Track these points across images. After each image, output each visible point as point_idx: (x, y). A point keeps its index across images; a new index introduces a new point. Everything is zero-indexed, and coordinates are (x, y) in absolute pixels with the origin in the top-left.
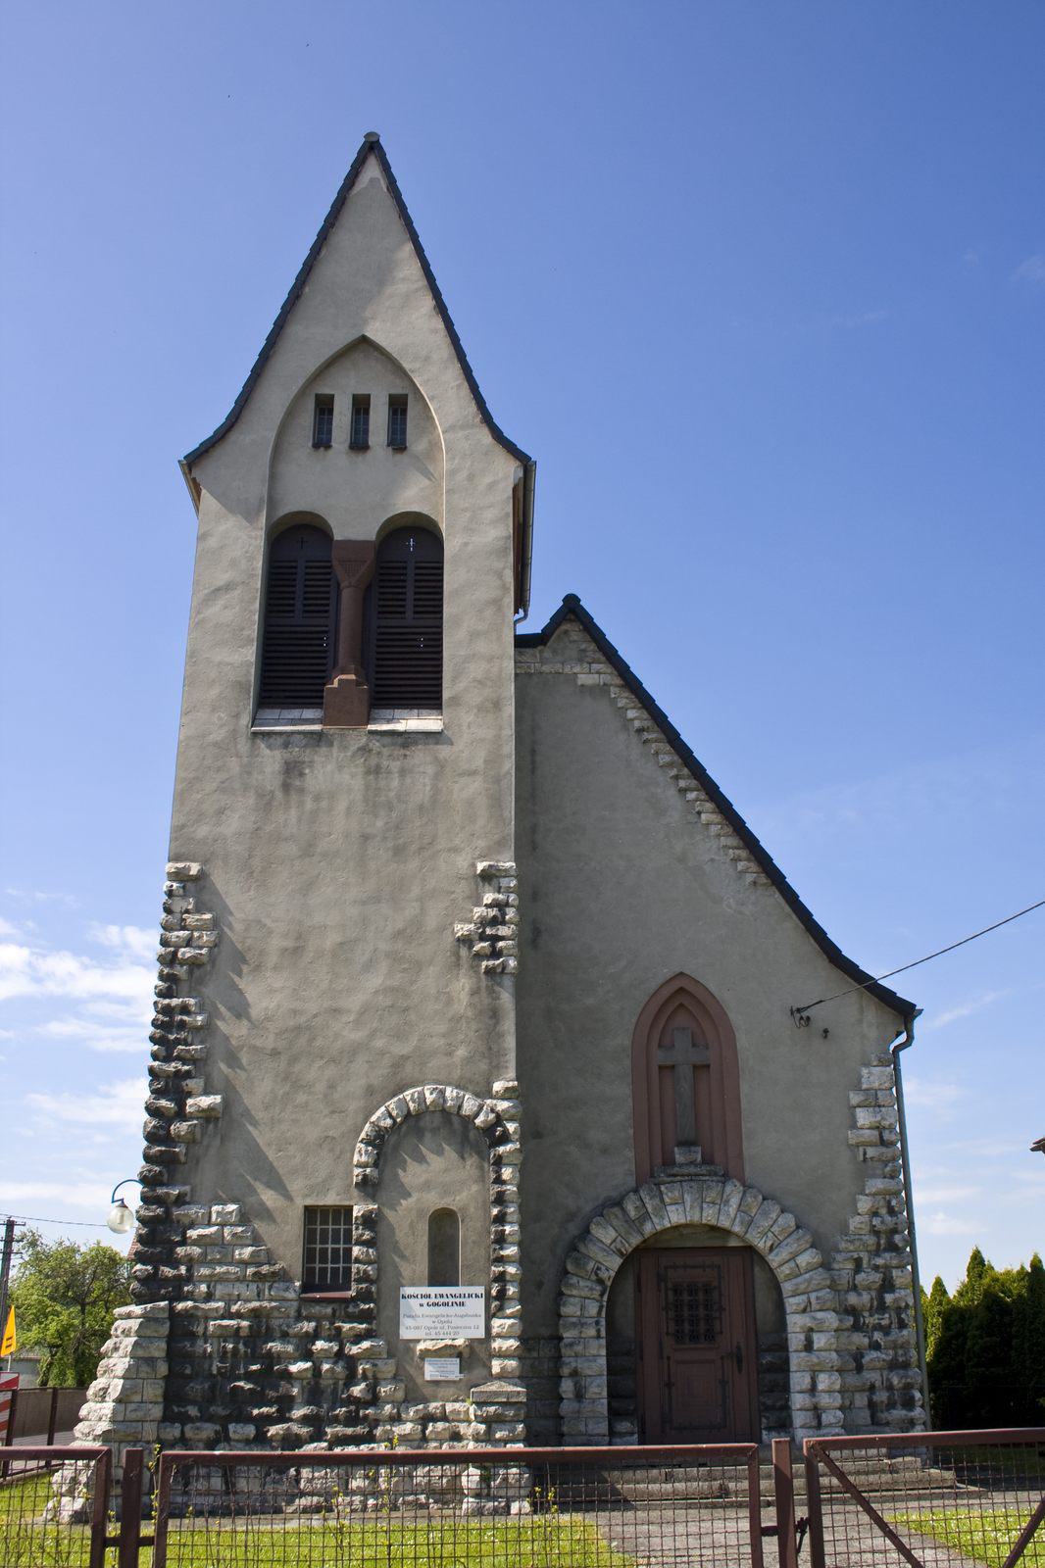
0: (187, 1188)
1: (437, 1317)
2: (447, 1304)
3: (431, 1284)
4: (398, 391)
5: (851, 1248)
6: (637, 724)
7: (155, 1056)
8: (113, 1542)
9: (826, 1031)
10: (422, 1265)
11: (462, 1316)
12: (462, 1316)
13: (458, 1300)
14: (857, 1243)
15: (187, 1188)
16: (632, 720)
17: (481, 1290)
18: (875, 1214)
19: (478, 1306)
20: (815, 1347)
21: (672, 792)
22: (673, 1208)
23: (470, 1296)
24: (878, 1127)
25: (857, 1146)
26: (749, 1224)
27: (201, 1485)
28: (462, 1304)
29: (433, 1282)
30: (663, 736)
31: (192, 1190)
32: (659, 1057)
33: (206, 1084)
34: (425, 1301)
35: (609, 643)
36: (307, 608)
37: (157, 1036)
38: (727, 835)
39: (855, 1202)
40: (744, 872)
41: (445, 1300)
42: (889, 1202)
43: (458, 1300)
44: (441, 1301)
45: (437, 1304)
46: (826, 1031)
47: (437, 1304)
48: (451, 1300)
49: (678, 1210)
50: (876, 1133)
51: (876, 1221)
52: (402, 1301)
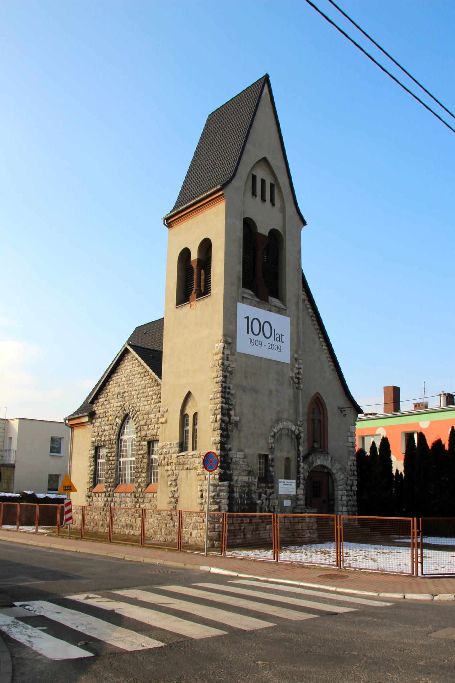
0: (231, 446)
2: (288, 485)
4: (272, 182)
6: (311, 314)
7: (222, 403)
10: (283, 474)
13: (291, 484)
15: (231, 446)
16: (310, 312)
17: (294, 481)
18: (351, 466)
19: (294, 485)
20: (343, 500)
21: (317, 337)
25: (349, 447)
26: (332, 466)
27: (239, 537)
28: (291, 485)
29: (285, 478)
31: (232, 446)
33: (235, 413)
34: (284, 483)
37: (223, 396)
38: (330, 358)
39: (347, 462)
40: (331, 365)
41: (288, 483)
42: (354, 463)
43: (291, 484)
46: (345, 415)
48: (289, 483)
49: (319, 461)
51: (352, 468)
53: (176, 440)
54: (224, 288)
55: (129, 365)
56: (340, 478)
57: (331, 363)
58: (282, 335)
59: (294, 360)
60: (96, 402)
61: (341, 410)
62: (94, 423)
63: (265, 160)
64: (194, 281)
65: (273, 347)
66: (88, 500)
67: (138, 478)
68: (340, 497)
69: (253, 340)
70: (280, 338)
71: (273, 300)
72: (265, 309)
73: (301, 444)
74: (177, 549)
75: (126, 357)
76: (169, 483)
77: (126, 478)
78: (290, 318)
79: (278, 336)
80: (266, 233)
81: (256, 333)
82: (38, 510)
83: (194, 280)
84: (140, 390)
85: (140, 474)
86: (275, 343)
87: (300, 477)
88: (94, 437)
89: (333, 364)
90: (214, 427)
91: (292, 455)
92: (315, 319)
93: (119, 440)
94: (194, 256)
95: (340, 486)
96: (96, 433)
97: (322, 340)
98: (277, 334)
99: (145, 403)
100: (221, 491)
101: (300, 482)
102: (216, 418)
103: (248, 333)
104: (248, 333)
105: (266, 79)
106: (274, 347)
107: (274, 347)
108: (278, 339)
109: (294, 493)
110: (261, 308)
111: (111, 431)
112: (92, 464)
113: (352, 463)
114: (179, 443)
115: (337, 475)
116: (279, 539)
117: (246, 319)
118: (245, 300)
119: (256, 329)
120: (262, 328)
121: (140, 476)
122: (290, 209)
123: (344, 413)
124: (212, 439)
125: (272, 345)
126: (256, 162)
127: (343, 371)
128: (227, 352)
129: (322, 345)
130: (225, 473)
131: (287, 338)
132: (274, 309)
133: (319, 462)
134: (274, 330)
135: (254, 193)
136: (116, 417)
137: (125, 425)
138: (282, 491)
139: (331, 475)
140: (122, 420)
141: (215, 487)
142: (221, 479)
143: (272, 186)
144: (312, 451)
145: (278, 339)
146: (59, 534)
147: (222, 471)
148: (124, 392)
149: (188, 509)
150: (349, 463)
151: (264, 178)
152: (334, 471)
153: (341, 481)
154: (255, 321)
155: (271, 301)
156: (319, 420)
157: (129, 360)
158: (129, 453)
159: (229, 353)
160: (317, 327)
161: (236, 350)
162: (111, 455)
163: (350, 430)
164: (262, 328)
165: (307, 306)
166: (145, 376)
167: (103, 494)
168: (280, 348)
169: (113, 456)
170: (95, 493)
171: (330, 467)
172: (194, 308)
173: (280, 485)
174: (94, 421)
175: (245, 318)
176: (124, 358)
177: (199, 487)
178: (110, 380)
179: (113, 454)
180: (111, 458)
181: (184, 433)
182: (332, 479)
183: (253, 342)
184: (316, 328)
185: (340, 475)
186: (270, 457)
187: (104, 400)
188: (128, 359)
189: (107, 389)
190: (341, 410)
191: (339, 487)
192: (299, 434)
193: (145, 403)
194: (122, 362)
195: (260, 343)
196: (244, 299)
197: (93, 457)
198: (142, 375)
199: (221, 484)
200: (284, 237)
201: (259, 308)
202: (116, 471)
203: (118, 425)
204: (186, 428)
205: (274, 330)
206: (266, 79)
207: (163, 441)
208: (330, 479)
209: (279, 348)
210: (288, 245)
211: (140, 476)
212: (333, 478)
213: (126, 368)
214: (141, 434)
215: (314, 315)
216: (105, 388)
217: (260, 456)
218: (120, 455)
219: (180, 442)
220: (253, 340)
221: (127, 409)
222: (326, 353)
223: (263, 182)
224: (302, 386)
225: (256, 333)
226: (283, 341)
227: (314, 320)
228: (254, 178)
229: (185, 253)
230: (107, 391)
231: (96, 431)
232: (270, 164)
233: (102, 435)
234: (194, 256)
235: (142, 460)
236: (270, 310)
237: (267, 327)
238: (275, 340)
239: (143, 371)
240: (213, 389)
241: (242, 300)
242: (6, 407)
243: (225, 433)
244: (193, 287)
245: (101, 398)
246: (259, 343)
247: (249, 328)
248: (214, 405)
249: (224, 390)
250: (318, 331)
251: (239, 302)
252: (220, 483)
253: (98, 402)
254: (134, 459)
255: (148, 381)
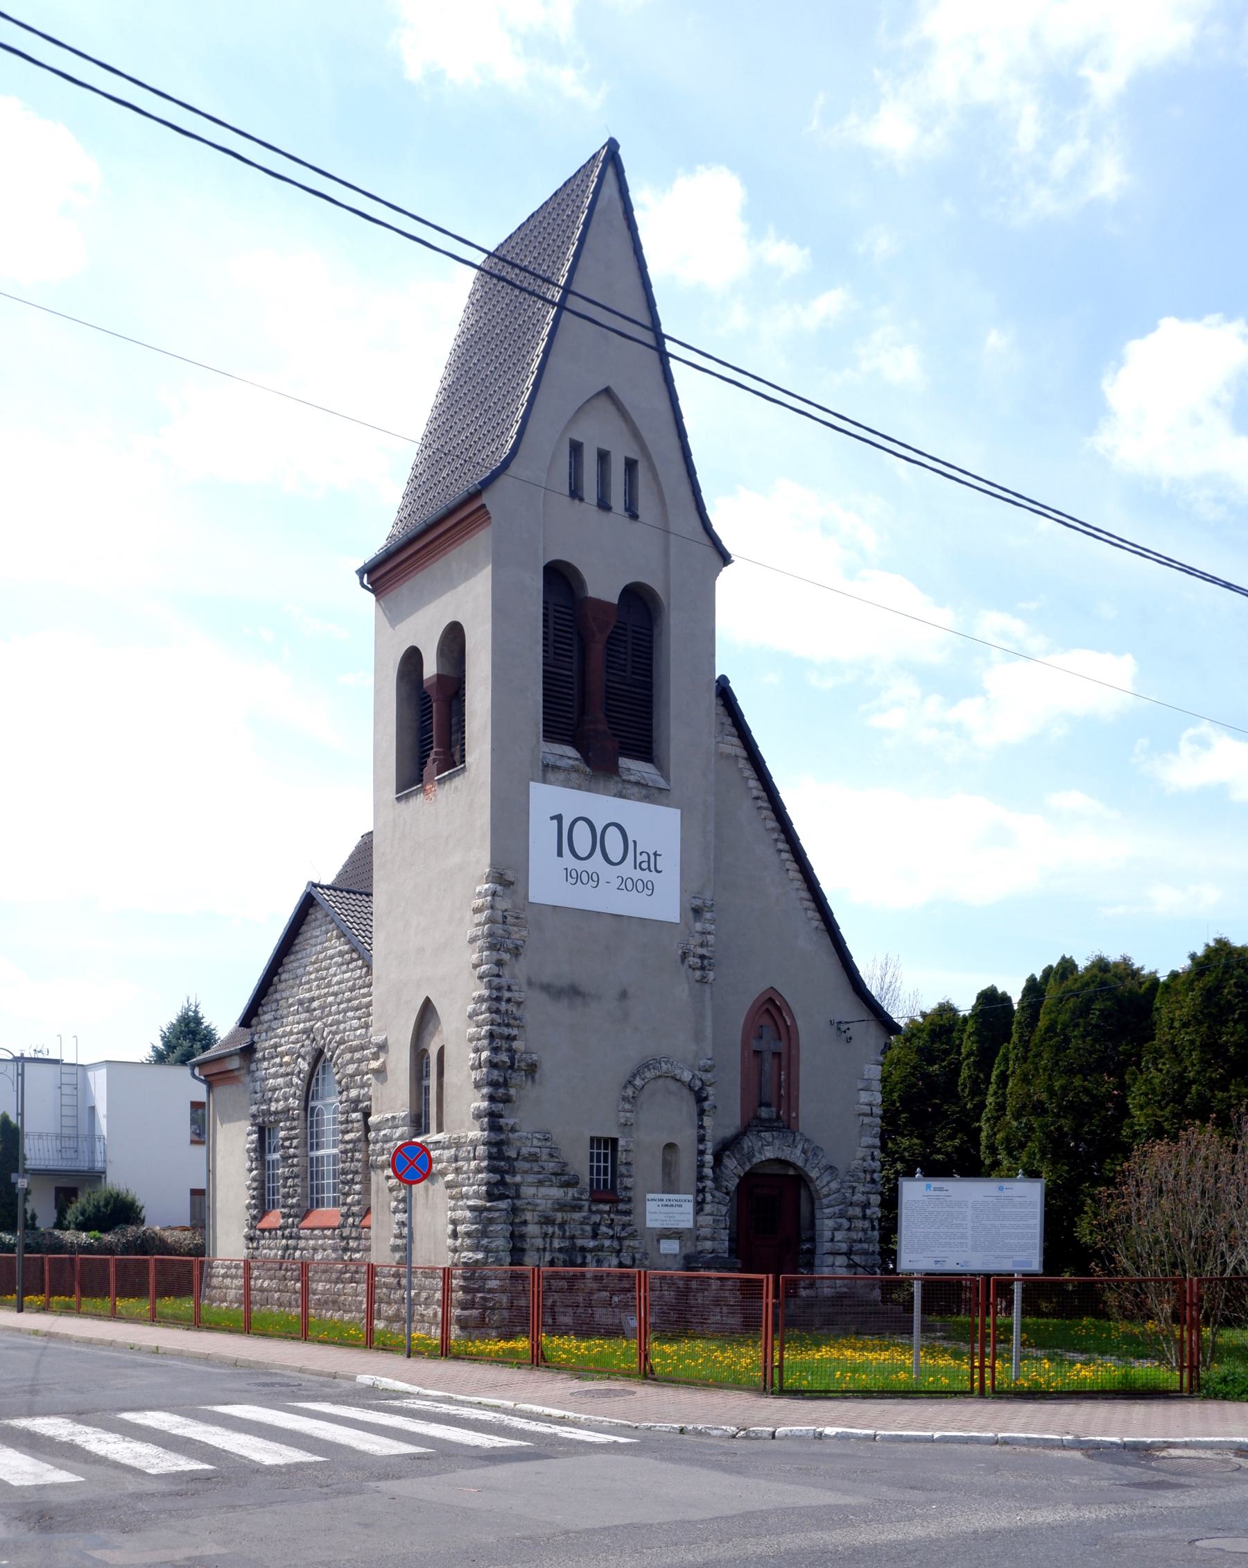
1: (667, 1213)
2: (672, 1206)
3: (663, 1192)
4: (632, 456)
5: (852, 1180)
6: (755, 793)
8: (777, 1366)
9: (851, 1038)
11: (681, 1213)
12: (681, 1213)
13: (679, 1203)
14: (856, 1177)
15: (517, 1120)
16: (751, 788)
17: (690, 1197)
19: (689, 1207)
20: (836, 1240)
22: (769, 1148)
23: (685, 1201)
24: (870, 1105)
28: (681, 1206)
30: (770, 806)
32: (755, 1045)
34: (660, 1203)
35: (492, 698)
36: (636, 653)
37: (494, 1007)
41: (671, 1203)
42: (873, 1153)
43: (679, 1203)
44: (669, 1203)
45: (667, 1205)
46: (851, 1038)
47: (667, 1205)
48: (674, 1203)
50: (869, 1108)
52: (647, 1202)
53: (404, 1109)
54: (493, 750)
55: (318, 933)
56: (830, 1190)
57: (811, 914)
58: (655, 854)
59: (691, 915)
60: (254, 1021)
61: (840, 1028)
62: (254, 1071)
63: (607, 392)
64: (434, 733)
65: (630, 886)
66: (250, 1246)
67: (347, 1194)
68: (828, 1234)
69: (573, 872)
70: (651, 862)
71: (633, 767)
72: (606, 792)
73: (706, 1113)
74: (300, 1336)
75: (311, 914)
76: (394, 1204)
77: (325, 1195)
78: (679, 811)
79: (645, 857)
80: (613, 597)
81: (583, 854)
82: (112, 1269)
83: (432, 731)
84: (344, 994)
85: (350, 1187)
86: (638, 874)
87: (704, 1187)
88: (256, 1104)
89: (817, 915)
90: (475, 1079)
91: (685, 1138)
92: (766, 805)
93: (307, 1108)
94: (430, 668)
95: (828, 1207)
96: (258, 1095)
97: (785, 856)
98: (641, 854)
99: (355, 1023)
100: (491, 1221)
101: (704, 1201)
102: (480, 1059)
103: (560, 854)
104: (560, 854)
105: (611, 156)
106: (635, 885)
107: (635, 885)
108: (645, 865)
109: (690, 1225)
110: (597, 792)
111: (288, 1090)
112: (254, 1166)
113: (869, 1153)
114: (411, 1117)
115: (821, 1182)
116: (764, 1333)
117: (555, 822)
118: (550, 776)
119: (583, 845)
120: (598, 841)
121: (350, 1189)
122: (687, 524)
123: (849, 1034)
124: (472, 1106)
125: (629, 880)
126: (596, 392)
127: (844, 931)
128: (502, 904)
129: (788, 870)
130: (502, 1182)
131: (671, 863)
132: (636, 790)
133: (769, 1154)
134: (635, 842)
135: (575, 493)
136: (298, 1057)
137: (318, 1074)
138: (656, 1220)
139: (805, 1182)
140: (309, 1064)
141: (477, 1213)
142: (490, 1196)
143: (631, 465)
144: (752, 1124)
145: (645, 865)
146: (198, 1323)
147: (495, 1177)
148: (312, 1000)
149: (430, 1261)
150: (861, 1153)
151: (605, 447)
152: (814, 1174)
153: (831, 1198)
154: (581, 824)
155: (629, 770)
156: (774, 1054)
157: (318, 923)
158: (328, 1138)
159: (509, 907)
160: (773, 824)
161: (526, 897)
162: (291, 1144)
163: (863, 1075)
164: (598, 841)
165: (743, 772)
166: (352, 960)
167: (278, 1232)
168: (651, 888)
169: (295, 1148)
170: (263, 1230)
171: (800, 1163)
172: (433, 798)
173: (651, 1207)
174: (253, 1067)
175: (552, 818)
176: (309, 917)
177: (449, 1213)
178: (280, 970)
179: (295, 1142)
180: (292, 1151)
181: (421, 1094)
182: (810, 1190)
183: (574, 874)
184: (768, 827)
185: (828, 1183)
186: (621, 1143)
187: (272, 1017)
188: (316, 920)
189: (276, 991)
190: (840, 1028)
191: (827, 1211)
192: (701, 1089)
193: (355, 1023)
194: (304, 928)
195: (595, 879)
196: (548, 771)
197: (255, 1150)
198: (347, 957)
199: (490, 1206)
200: (665, 603)
201: (589, 790)
202: (303, 1180)
203: (302, 1075)
204: (425, 1083)
205: (635, 842)
206: (611, 156)
207: (380, 1112)
208: (803, 1193)
209: (649, 887)
210: (675, 623)
211: (350, 1189)
212: (812, 1188)
213: (313, 941)
214: (348, 1095)
215: (763, 794)
216: (272, 989)
217: (595, 1142)
218: (312, 1144)
219: (413, 1113)
220: (573, 872)
221: (318, 1038)
222: (798, 889)
223: (603, 456)
224: (711, 975)
225: (583, 854)
226: (659, 869)
227: (765, 808)
228: (576, 449)
229: (412, 658)
230: (277, 996)
231: (258, 1089)
232: (622, 405)
233: (270, 1100)
234: (430, 668)
235: (353, 1156)
236: (621, 795)
237: (613, 837)
238: (635, 868)
239: (346, 947)
240: (474, 991)
241: (540, 773)
242: (75, 1036)
243: (502, 1091)
244: (432, 748)
245: (265, 1013)
246: (590, 877)
247: (564, 842)
248: (476, 1029)
249: (495, 994)
250: (775, 836)
251: (533, 780)
252: (488, 1204)
253: (260, 1023)
254: (336, 1151)
255: (359, 971)
